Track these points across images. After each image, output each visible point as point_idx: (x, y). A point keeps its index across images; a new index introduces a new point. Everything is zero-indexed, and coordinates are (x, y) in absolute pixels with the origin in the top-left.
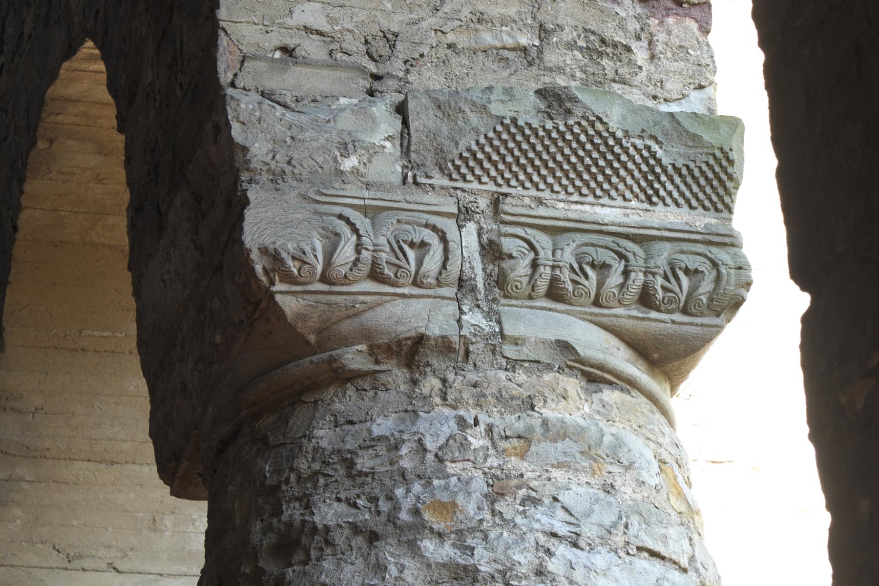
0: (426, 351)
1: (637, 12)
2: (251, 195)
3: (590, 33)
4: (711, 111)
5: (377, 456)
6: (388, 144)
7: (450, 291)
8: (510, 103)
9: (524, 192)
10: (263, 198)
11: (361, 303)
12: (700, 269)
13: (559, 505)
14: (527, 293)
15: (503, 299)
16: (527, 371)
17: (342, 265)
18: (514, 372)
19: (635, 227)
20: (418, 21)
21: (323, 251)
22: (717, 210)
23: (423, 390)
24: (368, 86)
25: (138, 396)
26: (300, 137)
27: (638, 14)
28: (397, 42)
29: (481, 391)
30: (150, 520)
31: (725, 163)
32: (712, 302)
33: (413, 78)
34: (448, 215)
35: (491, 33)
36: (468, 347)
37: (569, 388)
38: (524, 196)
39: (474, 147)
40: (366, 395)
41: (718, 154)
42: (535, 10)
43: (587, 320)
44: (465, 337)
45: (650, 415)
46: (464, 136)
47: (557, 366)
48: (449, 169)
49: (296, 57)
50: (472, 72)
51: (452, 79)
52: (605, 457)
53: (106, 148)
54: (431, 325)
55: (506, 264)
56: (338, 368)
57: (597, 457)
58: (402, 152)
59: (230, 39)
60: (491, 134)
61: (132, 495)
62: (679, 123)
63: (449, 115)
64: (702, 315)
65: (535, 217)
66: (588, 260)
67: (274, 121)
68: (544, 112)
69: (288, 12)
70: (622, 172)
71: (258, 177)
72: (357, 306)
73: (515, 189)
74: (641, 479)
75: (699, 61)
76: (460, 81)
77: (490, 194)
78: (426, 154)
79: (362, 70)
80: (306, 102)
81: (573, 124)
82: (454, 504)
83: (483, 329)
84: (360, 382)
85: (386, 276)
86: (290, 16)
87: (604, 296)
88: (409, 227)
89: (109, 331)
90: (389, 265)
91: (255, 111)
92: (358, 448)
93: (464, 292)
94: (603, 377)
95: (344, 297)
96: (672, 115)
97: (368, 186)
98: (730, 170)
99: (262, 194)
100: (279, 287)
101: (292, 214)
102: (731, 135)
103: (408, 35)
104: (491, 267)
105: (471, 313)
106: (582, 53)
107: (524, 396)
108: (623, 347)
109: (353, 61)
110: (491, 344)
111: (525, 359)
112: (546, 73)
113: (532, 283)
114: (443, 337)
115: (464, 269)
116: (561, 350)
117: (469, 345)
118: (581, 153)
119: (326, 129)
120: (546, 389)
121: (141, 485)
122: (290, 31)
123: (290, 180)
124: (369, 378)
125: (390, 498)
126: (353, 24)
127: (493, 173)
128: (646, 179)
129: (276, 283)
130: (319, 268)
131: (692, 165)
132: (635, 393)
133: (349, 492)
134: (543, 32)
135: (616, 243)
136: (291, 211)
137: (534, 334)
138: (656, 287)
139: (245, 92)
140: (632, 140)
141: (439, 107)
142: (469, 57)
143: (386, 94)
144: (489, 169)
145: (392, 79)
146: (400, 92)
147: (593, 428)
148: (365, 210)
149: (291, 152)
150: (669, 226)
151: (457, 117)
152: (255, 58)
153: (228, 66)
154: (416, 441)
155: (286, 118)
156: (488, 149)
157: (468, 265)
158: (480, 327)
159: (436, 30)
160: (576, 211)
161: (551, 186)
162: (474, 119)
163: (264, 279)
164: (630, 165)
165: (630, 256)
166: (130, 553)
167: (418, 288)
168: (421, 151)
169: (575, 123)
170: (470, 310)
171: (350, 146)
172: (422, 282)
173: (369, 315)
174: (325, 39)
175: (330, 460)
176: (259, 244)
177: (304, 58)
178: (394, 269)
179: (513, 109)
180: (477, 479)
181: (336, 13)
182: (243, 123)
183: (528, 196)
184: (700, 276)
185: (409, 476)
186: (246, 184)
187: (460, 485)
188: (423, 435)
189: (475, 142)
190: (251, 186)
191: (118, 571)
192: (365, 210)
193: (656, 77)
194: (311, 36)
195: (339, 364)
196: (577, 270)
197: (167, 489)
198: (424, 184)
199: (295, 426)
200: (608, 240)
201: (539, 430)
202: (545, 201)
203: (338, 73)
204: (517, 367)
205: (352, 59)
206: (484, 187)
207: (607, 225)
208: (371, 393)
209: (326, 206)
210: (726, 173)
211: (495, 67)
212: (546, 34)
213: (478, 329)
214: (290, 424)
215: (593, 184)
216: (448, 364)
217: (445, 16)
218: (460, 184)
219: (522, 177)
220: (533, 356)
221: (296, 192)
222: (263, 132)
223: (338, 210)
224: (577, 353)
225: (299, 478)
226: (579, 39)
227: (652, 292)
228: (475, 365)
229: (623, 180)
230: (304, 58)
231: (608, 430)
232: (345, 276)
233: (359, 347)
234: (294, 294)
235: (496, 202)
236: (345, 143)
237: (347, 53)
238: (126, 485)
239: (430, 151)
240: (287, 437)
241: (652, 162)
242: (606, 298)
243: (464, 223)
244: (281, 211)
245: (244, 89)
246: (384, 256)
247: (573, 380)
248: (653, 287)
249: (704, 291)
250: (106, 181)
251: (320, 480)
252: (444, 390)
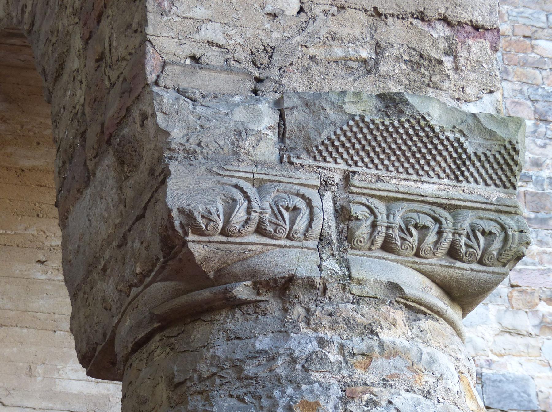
0: (295, 287)
1: (446, 34)
2: (172, 168)
3: (412, 50)
4: (498, 110)
5: (259, 365)
6: (269, 132)
7: (313, 243)
8: (359, 104)
9: (368, 171)
10: (181, 171)
11: (250, 251)
12: (493, 231)
13: (393, 406)
14: (368, 246)
15: (350, 250)
16: (369, 305)
17: (237, 223)
18: (359, 305)
19: (446, 198)
20: (289, 38)
21: (224, 212)
22: (505, 187)
23: (292, 316)
24: (253, 87)
25: (21, 278)
26: (207, 125)
27: (447, 36)
28: (274, 54)
29: (335, 319)
30: (27, 369)
31: (512, 153)
32: (501, 256)
33: (285, 81)
34: (313, 187)
35: (341, 48)
36: (326, 286)
37: (397, 318)
38: (367, 174)
39: (333, 137)
40: (250, 318)
42: (373, 32)
43: (409, 267)
44: (324, 278)
45: (452, 337)
46: (326, 128)
47: (389, 301)
48: (314, 153)
49: (201, 64)
50: (327, 77)
51: (313, 82)
52: (423, 370)
53: (11, 98)
54: (299, 268)
55: (352, 224)
56: (230, 298)
57: (418, 371)
58: (279, 138)
59: (154, 49)
60: (345, 128)
61: (15, 350)
62: (479, 121)
63: (314, 112)
64: (493, 265)
65: (375, 189)
66: (412, 223)
67: (188, 113)
68: (383, 111)
69: (196, 30)
70: (439, 158)
71: (176, 155)
72: (246, 252)
73: (361, 168)
74: (448, 387)
75: (491, 72)
76: (319, 84)
77: (343, 171)
78: (297, 140)
79: (249, 74)
80: (210, 98)
81: (404, 121)
82: (318, 404)
83: (336, 273)
84: (246, 308)
85: (268, 232)
86: (198, 33)
87: (423, 250)
88: (285, 196)
89: (3, 230)
90: (271, 224)
91: (174, 105)
92: (245, 358)
93: (323, 244)
95: (238, 246)
96: (474, 115)
97: (256, 163)
98: (516, 158)
99: (179, 167)
100: (191, 237)
101: (202, 183)
102: (517, 132)
103: (282, 48)
104: (342, 226)
105: (328, 260)
106: (406, 65)
107: (366, 324)
108: (434, 286)
109: (242, 67)
110: (342, 284)
111: (366, 295)
112: (380, 79)
113: (372, 238)
114: (308, 278)
115: (324, 227)
116: (392, 290)
117: (327, 284)
118: (410, 143)
119: (225, 120)
120: (381, 318)
121: (22, 343)
122: (197, 44)
123: (199, 158)
124: (252, 305)
125: (270, 397)
126: (243, 40)
127: (346, 156)
128: (455, 163)
129: (189, 234)
130: (221, 225)
131: (489, 154)
132: (441, 320)
133: (238, 390)
134: (379, 49)
135: (432, 210)
136: (201, 181)
137: (373, 277)
138: (461, 244)
139: (166, 90)
140: (446, 134)
141: (307, 105)
142: (325, 66)
143: (266, 93)
144: (343, 153)
145: (270, 82)
146: (276, 92)
147: (415, 348)
148: (252, 181)
149: (200, 137)
151: (320, 114)
152: (173, 63)
153: (153, 70)
154: (288, 355)
155: (197, 111)
156: (343, 138)
157: (327, 225)
158: (334, 271)
159: (302, 45)
160: (404, 185)
161: (387, 167)
162: (333, 115)
163: (180, 231)
164: (445, 153)
165: (443, 220)
166: (12, 392)
167: (290, 241)
168: (293, 138)
169: (406, 120)
170: (327, 258)
171: (243, 133)
172: (294, 237)
173: (255, 259)
174: (222, 50)
175: (225, 366)
176: (178, 206)
177: (207, 64)
178: (274, 227)
179: (360, 108)
180: (334, 385)
181: (231, 31)
182: (165, 114)
183: (370, 174)
184: (493, 236)
185: (284, 382)
186: (168, 160)
187: (321, 389)
188: (294, 351)
189: (333, 133)
190: (172, 161)
191: (4, 405)
192: (252, 181)
193: (460, 84)
194: (212, 48)
195: (231, 295)
196: (405, 230)
197: (84, 371)
198: (296, 163)
199: (196, 338)
200: (427, 208)
201: (377, 350)
202: (382, 178)
203: (232, 76)
204: (360, 301)
205: (242, 66)
206: (339, 166)
208: (254, 317)
209: (226, 178)
210: (513, 159)
211: (343, 73)
212: (380, 49)
213: (333, 272)
214: (192, 337)
215: (417, 166)
216: (311, 297)
217: (308, 35)
218: (322, 164)
219: (366, 160)
220: (372, 294)
221: (205, 167)
222: (180, 121)
223: (235, 181)
224: (404, 292)
225: (200, 377)
226: (404, 54)
227: (458, 248)
228: (330, 299)
229: (439, 164)
230: (207, 64)
231: (426, 350)
232: (239, 231)
233: (246, 283)
234: (202, 243)
235: (347, 177)
236: (240, 131)
237: (238, 61)
238: (11, 342)
239: (300, 138)
240: (190, 346)
241: (460, 150)
242: (425, 251)
243: (323, 193)
244: (194, 181)
245: (165, 87)
246: (267, 216)
247: (400, 312)
248: (459, 244)
250: (8, 121)
251: (217, 380)
252: (308, 317)
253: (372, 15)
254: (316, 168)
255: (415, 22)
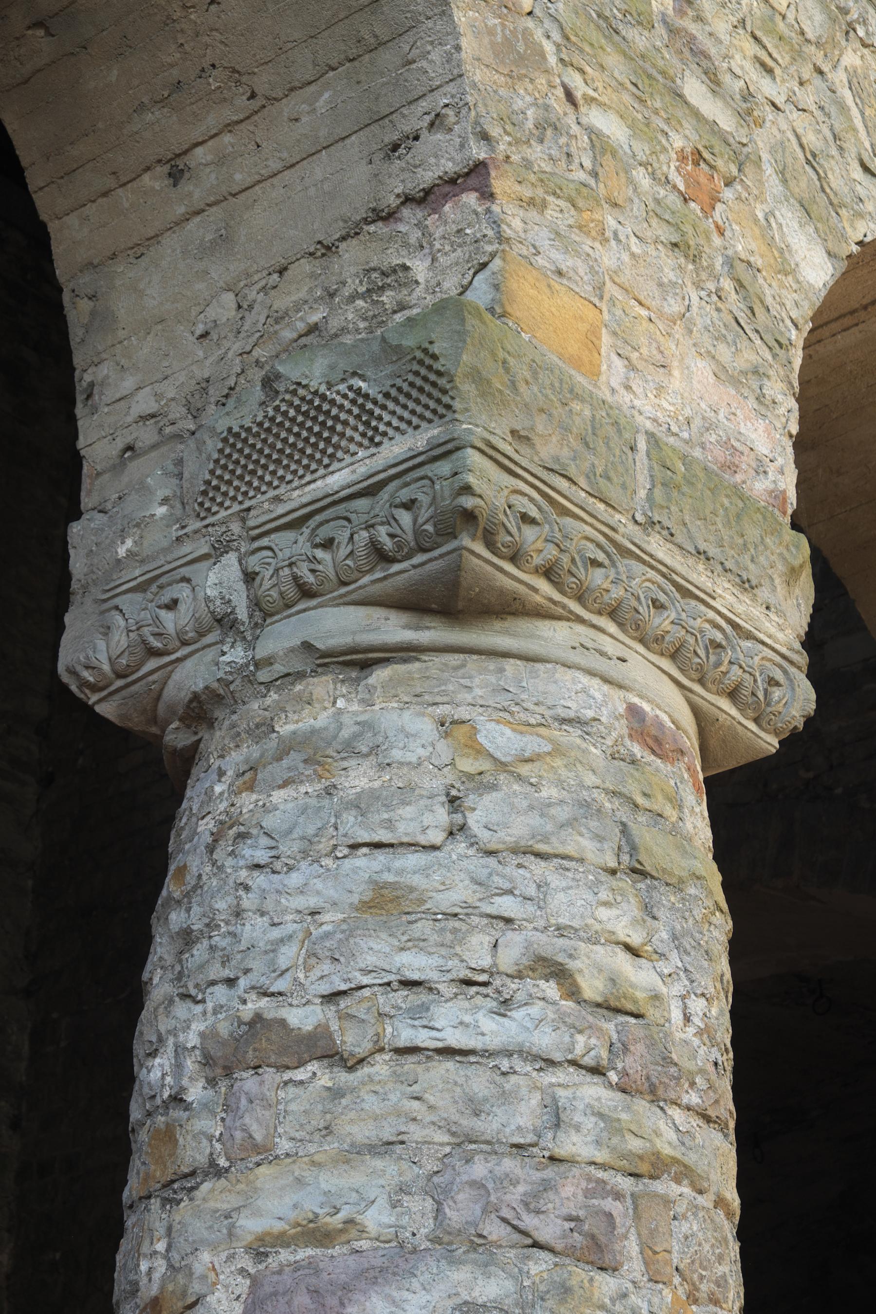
16: (279, 689)
41: (419, 354)
94: (371, 659)
98: (437, 366)
131: (399, 382)
150: (392, 462)
207: (337, 492)
233: (173, 726)
249: (424, 519)
253: (323, 255)
254: (204, 530)
255: (372, 228)
